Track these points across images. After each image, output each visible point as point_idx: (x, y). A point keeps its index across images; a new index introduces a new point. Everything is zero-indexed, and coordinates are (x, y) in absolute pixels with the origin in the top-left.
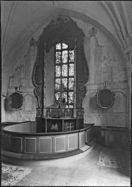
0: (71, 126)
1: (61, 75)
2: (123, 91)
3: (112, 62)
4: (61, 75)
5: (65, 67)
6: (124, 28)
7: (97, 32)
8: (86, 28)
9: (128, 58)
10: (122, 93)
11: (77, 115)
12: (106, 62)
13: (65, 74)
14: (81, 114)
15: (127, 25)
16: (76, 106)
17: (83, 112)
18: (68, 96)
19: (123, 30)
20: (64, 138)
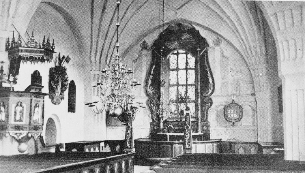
0: (153, 72)
1: (178, 83)
2: (251, 104)
3: (239, 74)
4: (178, 83)
5: (182, 73)
6: (247, 48)
7: (222, 43)
8: (210, 39)
9: (258, 12)
10: (250, 106)
11: (203, 130)
12: (233, 74)
13: (182, 81)
14: (207, 129)
15: (244, 141)
16: (201, 120)
17: (209, 126)
18: (187, 109)
19: (248, 49)
20: (167, 141)
